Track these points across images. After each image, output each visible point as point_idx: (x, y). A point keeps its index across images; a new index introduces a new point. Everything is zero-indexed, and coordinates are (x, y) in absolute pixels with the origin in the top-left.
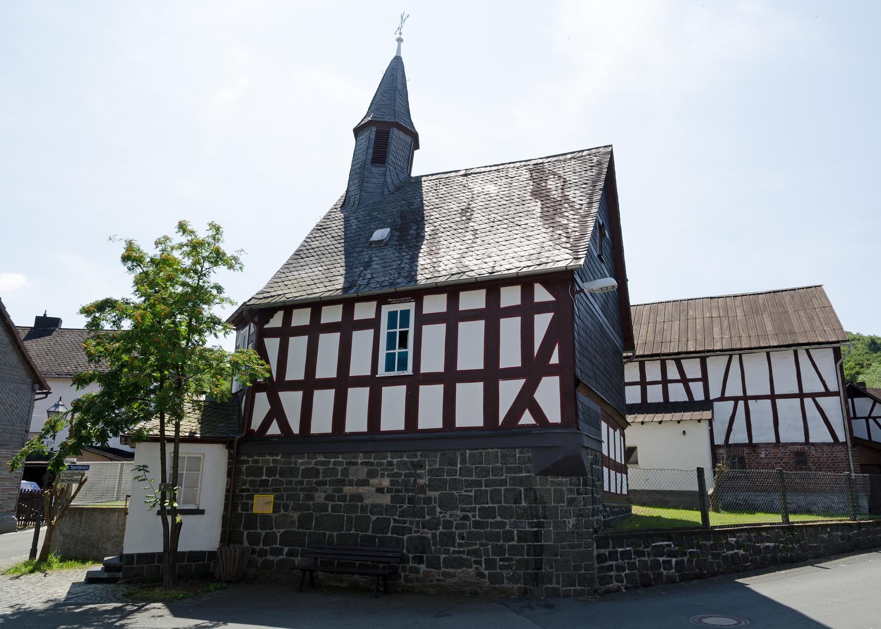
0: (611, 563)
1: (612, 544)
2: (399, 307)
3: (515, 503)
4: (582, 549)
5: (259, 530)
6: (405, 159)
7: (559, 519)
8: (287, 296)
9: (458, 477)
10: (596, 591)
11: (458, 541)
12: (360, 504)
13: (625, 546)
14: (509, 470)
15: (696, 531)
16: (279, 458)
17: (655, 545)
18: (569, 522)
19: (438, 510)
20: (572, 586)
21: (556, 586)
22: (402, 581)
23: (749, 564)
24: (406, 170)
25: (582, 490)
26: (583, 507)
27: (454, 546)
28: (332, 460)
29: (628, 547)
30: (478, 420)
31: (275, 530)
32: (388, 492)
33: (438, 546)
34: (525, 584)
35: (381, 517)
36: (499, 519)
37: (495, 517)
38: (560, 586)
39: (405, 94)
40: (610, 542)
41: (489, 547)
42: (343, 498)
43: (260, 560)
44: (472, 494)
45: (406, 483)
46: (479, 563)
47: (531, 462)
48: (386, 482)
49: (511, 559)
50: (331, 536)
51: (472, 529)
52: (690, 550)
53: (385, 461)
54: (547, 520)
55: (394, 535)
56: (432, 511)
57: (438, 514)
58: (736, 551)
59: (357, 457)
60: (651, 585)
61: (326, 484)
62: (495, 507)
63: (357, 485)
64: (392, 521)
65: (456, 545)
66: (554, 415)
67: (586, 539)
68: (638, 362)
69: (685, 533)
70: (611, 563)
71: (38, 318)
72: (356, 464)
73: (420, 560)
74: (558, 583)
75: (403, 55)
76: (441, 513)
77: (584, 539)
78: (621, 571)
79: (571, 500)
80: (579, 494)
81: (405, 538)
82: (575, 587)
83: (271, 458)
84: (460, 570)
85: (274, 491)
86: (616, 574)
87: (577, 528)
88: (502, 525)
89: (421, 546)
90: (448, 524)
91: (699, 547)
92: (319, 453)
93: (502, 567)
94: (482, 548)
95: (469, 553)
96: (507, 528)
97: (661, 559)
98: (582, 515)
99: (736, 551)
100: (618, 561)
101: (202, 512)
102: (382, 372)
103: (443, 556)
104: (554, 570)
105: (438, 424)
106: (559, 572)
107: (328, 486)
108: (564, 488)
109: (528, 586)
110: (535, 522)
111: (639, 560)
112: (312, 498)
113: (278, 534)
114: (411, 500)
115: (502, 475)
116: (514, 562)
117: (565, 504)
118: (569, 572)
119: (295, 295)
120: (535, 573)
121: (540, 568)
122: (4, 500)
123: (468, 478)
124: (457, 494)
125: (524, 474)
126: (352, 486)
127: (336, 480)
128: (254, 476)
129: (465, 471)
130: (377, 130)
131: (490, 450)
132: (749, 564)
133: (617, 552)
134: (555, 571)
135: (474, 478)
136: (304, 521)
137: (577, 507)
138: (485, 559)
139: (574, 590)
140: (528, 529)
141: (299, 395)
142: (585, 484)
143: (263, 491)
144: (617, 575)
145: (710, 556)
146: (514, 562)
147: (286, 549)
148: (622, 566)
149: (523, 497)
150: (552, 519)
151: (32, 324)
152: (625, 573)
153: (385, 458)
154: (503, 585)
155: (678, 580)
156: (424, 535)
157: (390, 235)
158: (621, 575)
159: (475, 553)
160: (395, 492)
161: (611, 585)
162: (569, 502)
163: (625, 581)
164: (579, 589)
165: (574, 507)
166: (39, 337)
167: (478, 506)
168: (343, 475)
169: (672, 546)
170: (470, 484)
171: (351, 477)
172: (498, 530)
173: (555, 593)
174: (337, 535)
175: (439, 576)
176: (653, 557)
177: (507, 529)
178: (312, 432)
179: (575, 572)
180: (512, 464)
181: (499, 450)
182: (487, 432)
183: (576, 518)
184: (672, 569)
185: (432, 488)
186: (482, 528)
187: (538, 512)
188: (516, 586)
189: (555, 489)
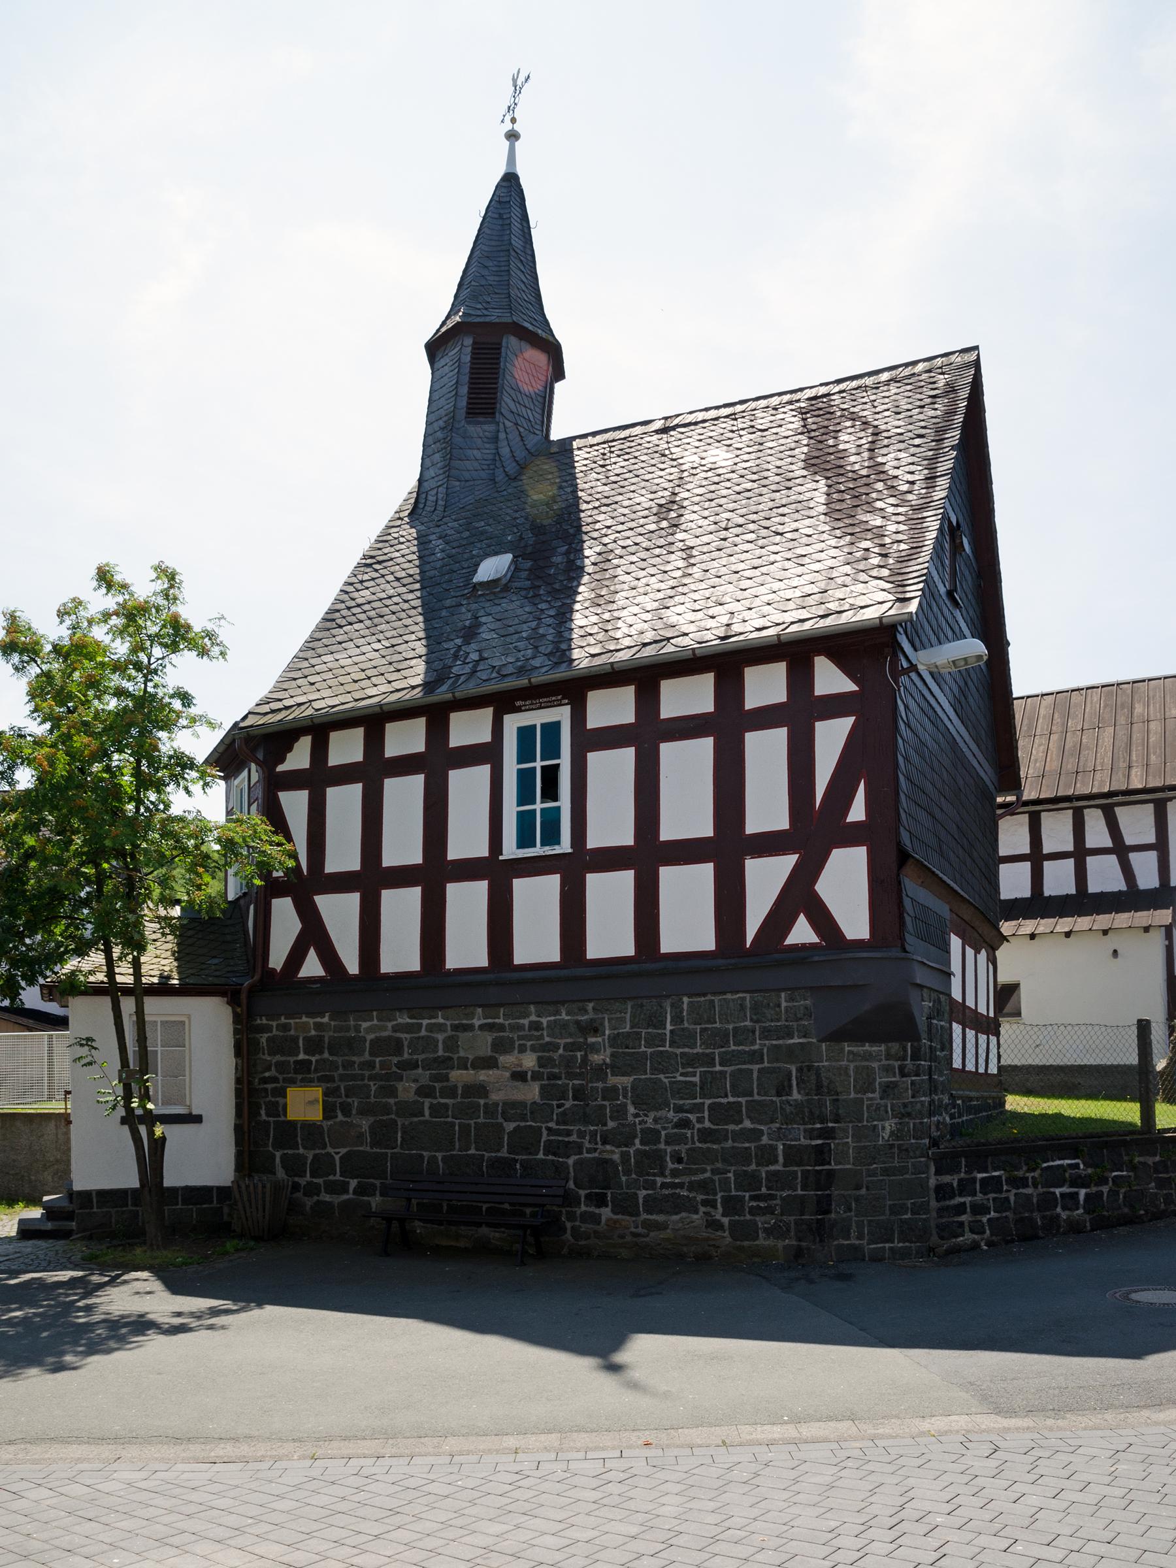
0: (962, 1200)
1: (966, 1166)
2: (537, 718)
3: (779, 1094)
4: (907, 1176)
5: (301, 1151)
6: (537, 403)
8: (317, 705)
9: (667, 1048)
10: (931, 1250)
11: (670, 1165)
12: (482, 1102)
14: (767, 1034)
15: (1128, 1138)
16: (326, 1020)
17: (1049, 1167)
18: (883, 1128)
19: (631, 1110)
20: (887, 1241)
21: (857, 1242)
22: (568, 1236)
25: (911, 1067)
27: (662, 1174)
28: (425, 1022)
29: (995, 1171)
31: (330, 1150)
32: (534, 1078)
35: (523, 1124)
36: (747, 1124)
40: (961, 1162)
41: (731, 1175)
42: (451, 1092)
43: (309, 1202)
44: (697, 1079)
45: (568, 1062)
46: (712, 1204)
48: (529, 1061)
51: (698, 1144)
53: (526, 1022)
55: (550, 1157)
56: (620, 1112)
57: (630, 1118)
59: (472, 1016)
60: (1036, 1237)
62: (740, 1103)
63: (474, 1067)
64: (545, 1132)
65: (667, 1172)
67: (916, 1158)
68: (1027, 815)
70: (962, 1200)
72: (470, 1028)
73: (601, 1201)
74: (860, 1237)
76: (636, 1115)
77: (912, 1158)
79: (888, 1087)
80: (903, 1075)
83: (311, 1021)
84: (675, 1218)
87: (898, 1138)
88: (756, 1135)
90: (651, 1136)
91: (1133, 1167)
92: (400, 1010)
93: (753, 1211)
95: (692, 1187)
96: (765, 1140)
97: (1058, 1191)
98: (909, 1115)
101: (198, 1119)
102: (510, 849)
103: (642, 1193)
104: (853, 1213)
105: (481, 959)
107: (420, 1071)
108: (875, 1065)
109: (804, 1244)
112: (393, 1092)
114: (579, 1094)
115: (753, 1043)
116: (778, 1202)
117: (877, 1095)
118: (881, 1218)
120: (817, 1219)
123: (687, 1050)
124: (666, 1080)
125: (796, 1040)
126: (466, 1069)
128: (283, 1054)
129: (682, 1037)
130: (474, 343)
131: (729, 996)
133: (974, 1179)
135: (698, 1050)
136: (382, 1134)
137: (899, 1099)
141: (353, 900)
142: (915, 1057)
143: (302, 1080)
144: (973, 1222)
146: (778, 1202)
149: (794, 1083)
150: (851, 1122)
152: (988, 1216)
153: (526, 1016)
154: (757, 1242)
155: (1089, 1228)
159: (704, 1186)
162: (884, 1091)
165: (893, 1099)
167: (708, 1102)
168: (447, 1048)
169: (1082, 1166)
170: (691, 1061)
171: (462, 1054)
172: (747, 1145)
173: (855, 1253)
177: (763, 1142)
179: (893, 1218)
180: (772, 1021)
181: (748, 996)
182: (721, 962)
184: (1077, 1209)
185: (617, 1070)
187: (823, 1109)
188: (780, 1244)
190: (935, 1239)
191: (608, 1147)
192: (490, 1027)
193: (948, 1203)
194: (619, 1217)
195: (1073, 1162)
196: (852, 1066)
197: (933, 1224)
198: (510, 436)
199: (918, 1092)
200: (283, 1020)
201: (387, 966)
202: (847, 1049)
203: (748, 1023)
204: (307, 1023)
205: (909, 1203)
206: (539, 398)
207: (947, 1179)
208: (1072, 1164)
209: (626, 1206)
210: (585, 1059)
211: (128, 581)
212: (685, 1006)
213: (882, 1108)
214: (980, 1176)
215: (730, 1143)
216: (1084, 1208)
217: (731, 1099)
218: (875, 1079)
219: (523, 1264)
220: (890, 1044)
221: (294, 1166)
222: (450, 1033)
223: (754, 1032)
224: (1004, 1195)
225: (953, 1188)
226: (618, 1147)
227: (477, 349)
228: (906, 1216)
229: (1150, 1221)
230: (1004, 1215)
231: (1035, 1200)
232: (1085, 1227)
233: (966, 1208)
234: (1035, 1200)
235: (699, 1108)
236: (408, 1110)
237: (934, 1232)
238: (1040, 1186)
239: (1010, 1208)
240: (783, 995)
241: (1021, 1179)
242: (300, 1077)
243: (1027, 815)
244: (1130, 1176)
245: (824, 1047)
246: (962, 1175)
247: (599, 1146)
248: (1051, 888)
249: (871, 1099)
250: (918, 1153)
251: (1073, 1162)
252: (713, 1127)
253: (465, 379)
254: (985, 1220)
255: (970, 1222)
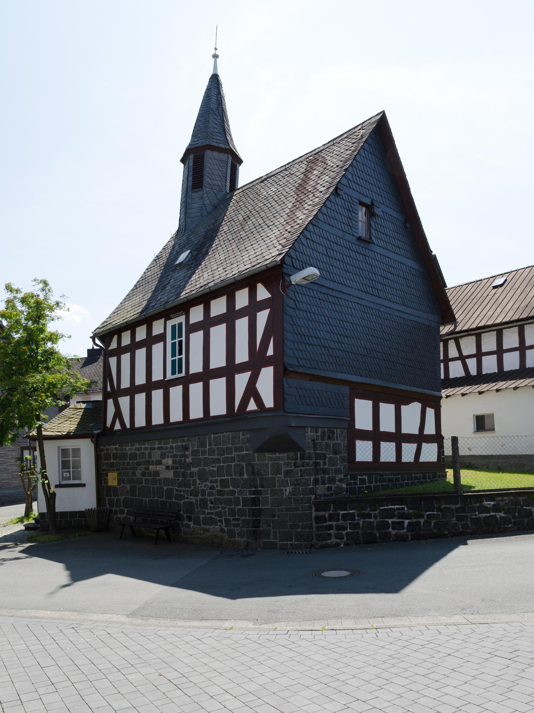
0: (330, 523)
1: (333, 508)
3: (240, 476)
4: (299, 512)
5: (113, 497)
6: (222, 177)
7: (277, 488)
8: (113, 323)
9: (207, 456)
10: (312, 546)
11: (210, 505)
12: (158, 478)
13: (348, 509)
14: (237, 449)
15: (437, 496)
16: (117, 446)
17: (384, 509)
18: (286, 490)
19: (198, 482)
20: (289, 541)
21: (273, 541)
22: (182, 533)
23: (510, 526)
24: (224, 188)
25: (300, 463)
26: (299, 477)
28: (143, 446)
29: (351, 510)
30: (223, 411)
32: (172, 469)
33: (199, 509)
34: (248, 538)
35: (169, 487)
36: (231, 488)
37: (229, 487)
38: (278, 540)
39: (220, 112)
40: (330, 506)
41: (227, 509)
43: (115, 517)
44: (216, 469)
46: (221, 521)
47: (249, 442)
48: (170, 462)
49: (239, 519)
50: (146, 500)
51: (217, 497)
52: (427, 513)
53: (169, 446)
54: (265, 489)
55: (176, 501)
56: (195, 482)
57: (198, 485)
58: (492, 514)
59: (154, 444)
60: (375, 542)
61: (141, 465)
62: (228, 479)
63: (156, 464)
64: (175, 490)
65: (209, 508)
66: (269, 402)
67: (302, 504)
68: (517, 327)
69: (422, 497)
70: (330, 523)
71: (89, 351)
74: (275, 538)
75: (219, 73)
76: (199, 484)
77: (300, 504)
78: (342, 530)
79: (288, 472)
80: (295, 466)
81: (182, 502)
82: (292, 541)
84: (211, 527)
85: (118, 469)
86: (335, 532)
87: (293, 495)
88: (232, 493)
89: (190, 507)
91: (439, 509)
92: (136, 442)
93: (235, 525)
94: (222, 510)
96: (236, 495)
97: (390, 521)
98: (299, 484)
99: (492, 514)
100: (339, 521)
101: (84, 485)
103: (202, 516)
104: (271, 528)
106: (267, 529)
107: (142, 466)
108: (282, 462)
109: (249, 540)
110: (253, 490)
111: (363, 522)
113: (122, 500)
115: (232, 454)
116: (241, 522)
117: (282, 476)
118: (286, 530)
119: (116, 322)
120: (253, 530)
121: (259, 527)
122: (10, 479)
123: (213, 457)
124: (207, 469)
126: (154, 465)
127: (146, 461)
129: (212, 451)
130: (194, 157)
131: (225, 434)
132: (510, 526)
133: (339, 514)
134: (273, 529)
135: (216, 457)
137: (293, 477)
138: (224, 519)
139: (290, 544)
140: (248, 496)
142: (302, 458)
143: (113, 470)
144: (337, 533)
145: (455, 519)
146: (241, 522)
147: (126, 510)
148: (343, 525)
149: (245, 470)
150: (269, 487)
151: (85, 355)
152: (346, 531)
153: (169, 443)
154: (235, 539)
155: (410, 539)
156: (191, 501)
157: (190, 256)
158: (342, 533)
159: (218, 514)
160: (175, 469)
161: (329, 541)
162: (286, 474)
163: (345, 538)
164: (297, 544)
165: (290, 477)
166: (90, 364)
167: (219, 478)
169: (406, 509)
171: (152, 459)
172: (231, 497)
173: (273, 546)
174: (149, 500)
175: (201, 530)
176: (380, 519)
177: (236, 496)
178: (136, 426)
179: (292, 530)
180: (237, 444)
181: (230, 433)
182: (228, 419)
183: (293, 487)
184: (403, 529)
186: (222, 495)
187: (255, 482)
189: (272, 464)
190: (315, 540)
191: (192, 497)
192: (159, 448)
193: (322, 524)
194: (195, 526)
195: (400, 507)
196: (270, 463)
197: (314, 534)
198: (209, 195)
199: (304, 474)
200: (107, 447)
201: (137, 425)
202: (267, 456)
203: (230, 445)
204: (113, 448)
205: (300, 524)
206: (224, 175)
207: (321, 513)
208: (400, 508)
209: (197, 522)
210: (185, 461)
211: (19, 288)
212: (212, 438)
213: (285, 481)
214: (342, 512)
215: (226, 496)
216: (407, 529)
217: (226, 477)
218: (281, 469)
219: (156, 543)
220: (289, 453)
221: (111, 502)
222: (149, 451)
223: (232, 449)
224: (356, 522)
225: (326, 518)
226: (194, 497)
227: (195, 159)
228: (298, 530)
229: (452, 537)
230: (356, 531)
231: (375, 525)
232: (408, 538)
233: (333, 527)
234: (375, 525)
235: (216, 481)
236: (140, 481)
237: (314, 537)
238: (378, 518)
239: (360, 528)
240: (241, 433)
241: (367, 514)
242: (112, 469)
243: (517, 327)
244: (439, 514)
245: (256, 455)
246: (331, 512)
247: (189, 496)
248: (507, 367)
249: (280, 477)
250: (304, 502)
251: (400, 507)
252: (221, 489)
253: (191, 173)
254: (344, 533)
255: (335, 534)
